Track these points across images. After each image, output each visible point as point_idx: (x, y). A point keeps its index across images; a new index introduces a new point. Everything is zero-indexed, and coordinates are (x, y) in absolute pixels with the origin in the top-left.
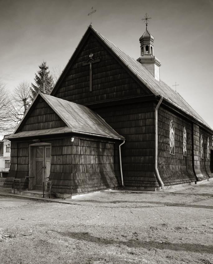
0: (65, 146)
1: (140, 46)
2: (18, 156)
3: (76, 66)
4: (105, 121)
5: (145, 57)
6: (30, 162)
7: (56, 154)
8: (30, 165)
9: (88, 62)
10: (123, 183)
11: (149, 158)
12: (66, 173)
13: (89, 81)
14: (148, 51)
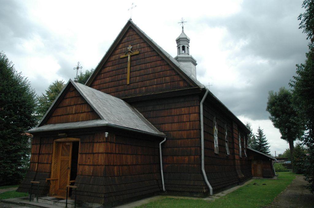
0: (97, 142)
1: (177, 46)
2: (41, 153)
3: (113, 58)
4: (143, 116)
5: (181, 56)
6: (53, 161)
7: (85, 152)
8: (53, 164)
9: (126, 54)
10: (164, 187)
11: (194, 158)
12: (189, 121)
13: (127, 73)
14: (184, 51)
